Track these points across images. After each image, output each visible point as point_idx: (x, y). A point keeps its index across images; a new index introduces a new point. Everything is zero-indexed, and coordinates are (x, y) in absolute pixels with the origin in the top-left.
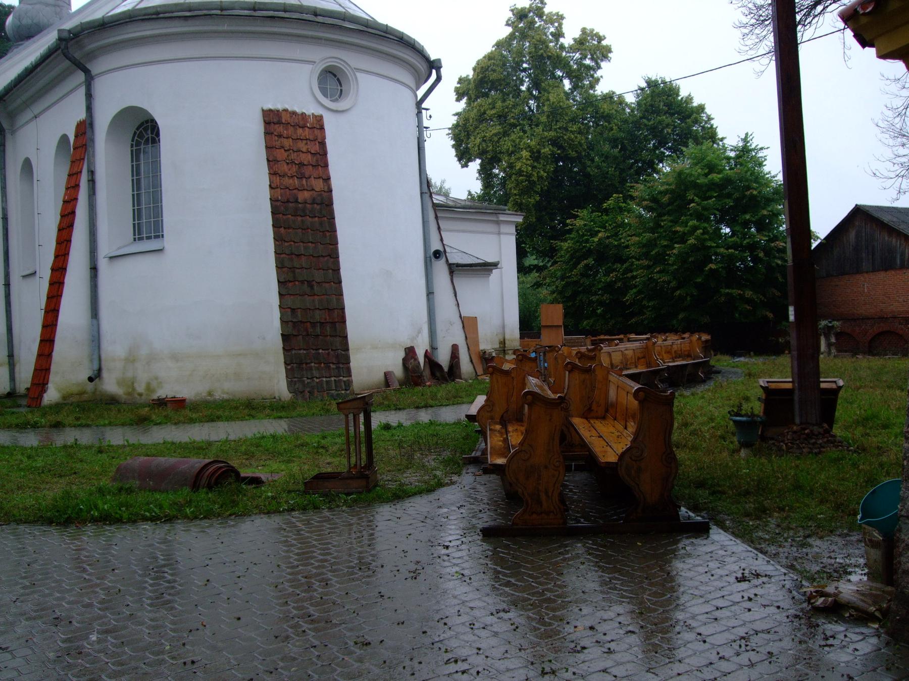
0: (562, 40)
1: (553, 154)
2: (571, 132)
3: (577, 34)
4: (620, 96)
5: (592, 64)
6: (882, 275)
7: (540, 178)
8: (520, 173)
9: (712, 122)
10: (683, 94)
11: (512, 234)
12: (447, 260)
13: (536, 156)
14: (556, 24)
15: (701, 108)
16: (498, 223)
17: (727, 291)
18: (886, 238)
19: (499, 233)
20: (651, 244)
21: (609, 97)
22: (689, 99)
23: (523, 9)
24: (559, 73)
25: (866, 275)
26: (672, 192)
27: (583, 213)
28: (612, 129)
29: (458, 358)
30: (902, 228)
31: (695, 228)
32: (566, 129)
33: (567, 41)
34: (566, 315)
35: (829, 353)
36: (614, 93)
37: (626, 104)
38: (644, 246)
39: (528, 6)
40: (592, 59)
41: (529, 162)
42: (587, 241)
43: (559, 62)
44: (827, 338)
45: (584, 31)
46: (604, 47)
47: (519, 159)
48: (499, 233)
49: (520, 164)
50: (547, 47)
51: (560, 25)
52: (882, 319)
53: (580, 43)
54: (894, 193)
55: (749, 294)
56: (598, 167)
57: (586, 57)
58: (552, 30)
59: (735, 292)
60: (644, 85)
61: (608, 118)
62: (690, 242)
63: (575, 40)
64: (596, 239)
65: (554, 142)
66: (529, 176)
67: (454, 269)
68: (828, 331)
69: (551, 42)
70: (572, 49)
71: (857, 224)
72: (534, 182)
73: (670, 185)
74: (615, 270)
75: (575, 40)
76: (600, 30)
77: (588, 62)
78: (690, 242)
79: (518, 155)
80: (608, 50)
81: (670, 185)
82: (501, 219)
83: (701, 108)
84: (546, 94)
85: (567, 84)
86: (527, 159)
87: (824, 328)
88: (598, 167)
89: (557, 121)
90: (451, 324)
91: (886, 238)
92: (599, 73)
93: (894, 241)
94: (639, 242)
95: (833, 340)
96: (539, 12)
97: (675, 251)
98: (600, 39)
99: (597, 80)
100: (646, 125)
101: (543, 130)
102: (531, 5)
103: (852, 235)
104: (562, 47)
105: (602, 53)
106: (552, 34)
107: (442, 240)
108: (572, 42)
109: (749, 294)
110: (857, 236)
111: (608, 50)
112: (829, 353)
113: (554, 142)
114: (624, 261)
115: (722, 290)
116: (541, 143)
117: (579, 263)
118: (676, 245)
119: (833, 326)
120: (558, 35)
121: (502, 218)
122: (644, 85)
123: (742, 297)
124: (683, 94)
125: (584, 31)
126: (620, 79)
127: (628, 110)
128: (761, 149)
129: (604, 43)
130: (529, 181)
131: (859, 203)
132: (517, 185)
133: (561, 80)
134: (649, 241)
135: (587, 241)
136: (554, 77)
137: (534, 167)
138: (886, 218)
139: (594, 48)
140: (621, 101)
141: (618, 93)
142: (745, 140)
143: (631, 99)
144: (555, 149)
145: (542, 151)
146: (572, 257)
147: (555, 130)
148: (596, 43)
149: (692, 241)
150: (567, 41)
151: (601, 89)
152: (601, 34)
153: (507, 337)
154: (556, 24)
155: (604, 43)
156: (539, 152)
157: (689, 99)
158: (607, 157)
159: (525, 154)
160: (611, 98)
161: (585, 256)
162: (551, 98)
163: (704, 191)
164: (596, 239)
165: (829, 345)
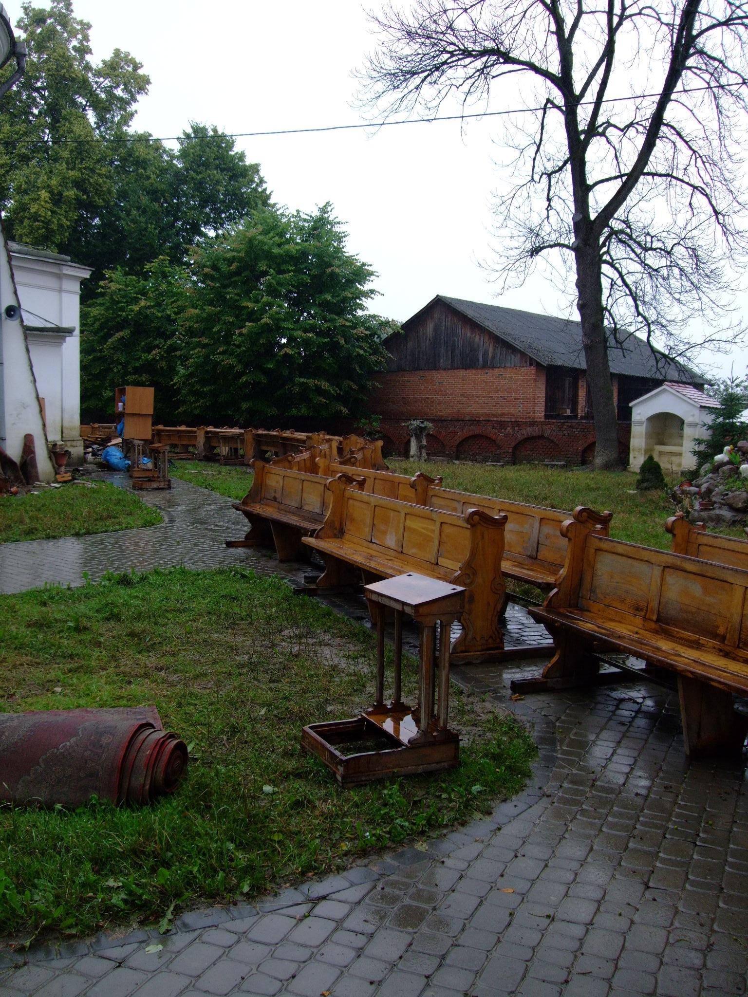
0: (88, 57)
1: (77, 199)
2: (99, 175)
3: (108, 56)
4: (158, 140)
5: (125, 96)
6: (461, 373)
7: (61, 226)
8: (35, 217)
9: (264, 186)
10: (237, 149)
11: (75, 293)
12: (22, 321)
13: (57, 199)
14: (80, 37)
15: (255, 168)
16: (59, 277)
17: (302, 380)
18: (469, 335)
19: (60, 291)
20: (212, 319)
21: (144, 139)
22: (241, 157)
23: (42, 11)
24: (81, 100)
25: (443, 372)
26: (240, 260)
27: (117, 275)
28: (148, 178)
29: (33, 452)
30: (487, 324)
31: (271, 305)
32: (93, 170)
33: (95, 60)
34: (156, 400)
35: (420, 456)
36: (150, 135)
37: (165, 151)
38: (203, 320)
39: (48, 9)
40: (126, 89)
41: (48, 206)
42: (122, 309)
43: (84, 87)
44: (419, 439)
45: (117, 52)
46: (140, 76)
47: (34, 200)
48: (60, 291)
49: (36, 206)
50: (71, 66)
51: (86, 38)
52: (475, 421)
53: (112, 68)
54: (497, 287)
55: (325, 385)
56: (134, 221)
57: (118, 86)
58: (75, 43)
59: (311, 382)
60: (190, 131)
61: (141, 163)
62: (263, 321)
63: (104, 62)
64: (136, 308)
65: (78, 184)
66: (47, 223)
67: (30, 332)
68: (419, 432)
69: (75, 59)
70: (98, 73)
71: (436, 316)
72: (53, 231)
73: (238, 252)
74: (157, 347)
75: (104, 62)
76: (137, 55)
77: (119, 92)
78: (263, 321)
79: (33, 196)
80: (146, 81)
81: (238, 252)
82: (65, 272)
83: (255, 168)
84: (67, 125)
85: (91, 117)
86: (46, 202)
87: (416, 429)
88: (134, 221)
89: (82, 159)
90: (24, 406)
91: (469, 335)
92: (134, 107)
93: (478, 339)
94: (198, 316)
95: (424, 443)
96: (64, 19)
97: (244, 331)
98: (136, 66)
99: (132, 115)
100: (193, 178)
101: (68, 169)
102: (52, 9)
103: (430, 328)
104: (88, 67)
105: (139, 84)
106: (74, 48)
107: (15, 293)
108: (101, 65)
109: (325, 385)
110: (436, 330)
111: (146, 81)
112: (420, 456)
113: (78, 184)
114: (167, 338)
115: (297, 380)
116: (64, 182)
117: (111, 336)
118: (247, 324)
119: (425, 427)
120: (83, 50)
121: (67, 271)
122: (190, 131)
123: (319, 391)
124: (237, 149)
125: (117, 52)
126: (160, 120)
127: (166, 158)
128: (339, 223)
129: (141, 72)
130: (47, 229)
131: (452, 292)
132: (31, 232)
133: (84, 110)
134: (210, 315)
135: (122, 309)
136: (74, 103)
137: (53, 212)
138: (470, 313)
139: (127, 75)
140: (157, 146)
141: (155, 137)
142: (323, 210)
143: (175, 147)
144: (80, 194)
145: (65, 194)
146: (102, 327)
147: (80, 169)
148: (130, 69)
149: (265, 320)
150: (95, 60)
151: (135, 128)
152: (138, 61)
153: (66, 424)
154: (80, 37)
155: (141, 72)
156: (60, 194)
157: (241, 157)
158: (144, 212)
159: (44, 194)
160: (148, 140)
161: (119, 327)
162: (75, 129)
163: (281, 262)
164: (136, 308)
165: (420, 448)
